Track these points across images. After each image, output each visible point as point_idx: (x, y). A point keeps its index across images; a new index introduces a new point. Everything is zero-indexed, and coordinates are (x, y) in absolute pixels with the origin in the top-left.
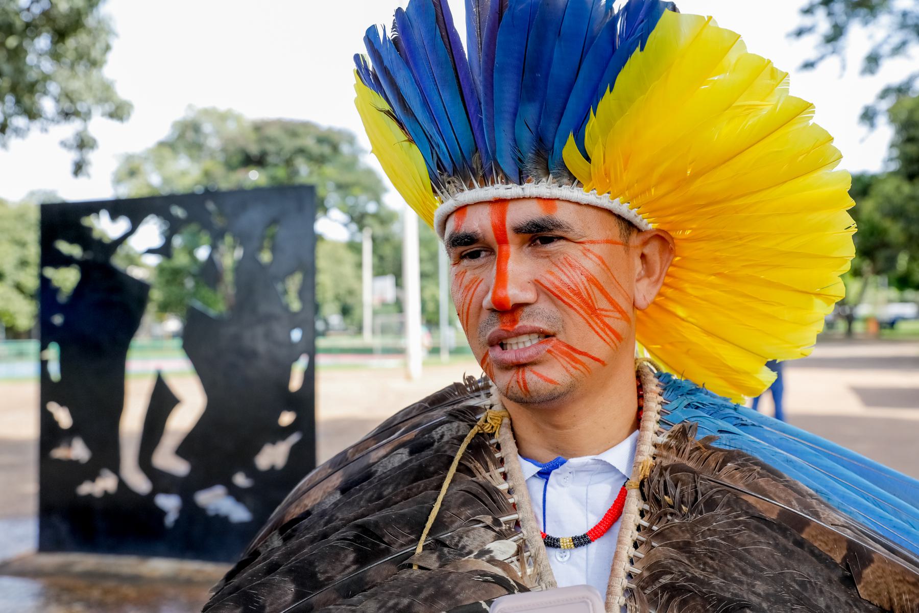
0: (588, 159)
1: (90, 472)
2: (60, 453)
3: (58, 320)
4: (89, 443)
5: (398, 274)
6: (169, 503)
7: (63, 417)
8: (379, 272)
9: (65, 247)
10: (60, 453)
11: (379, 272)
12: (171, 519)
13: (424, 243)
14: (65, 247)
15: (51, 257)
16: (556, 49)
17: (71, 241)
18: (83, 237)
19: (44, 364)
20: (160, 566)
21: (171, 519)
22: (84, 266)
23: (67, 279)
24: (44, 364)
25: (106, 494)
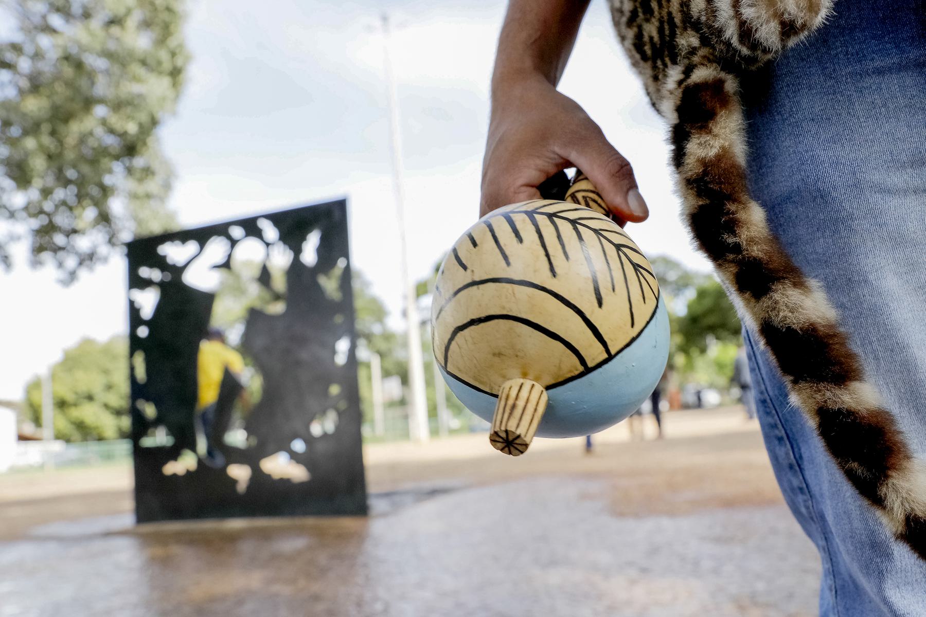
0: (567, 257)
1: (173, 453)
2: (148, 442)
3: (143, 332)
4: (171, 431)
5: (405, 380)
6: (240, 473)
7: (150, 411)
8: (386, 374)
9: (145, 272)
10: (148, 442)
11: (386, 374)
12: (242, 487)
13: (427, 368)
14: (145, 272)
15: (136, 282)
16: (591, 253)
17: (151, 266)
18: (161, 263)
19: (132, 369)
20: (236, 524)
21: (242, 487)
22: (163, 286)
23: (148, 301)
24: (132, 369)
25: (189, 473)
